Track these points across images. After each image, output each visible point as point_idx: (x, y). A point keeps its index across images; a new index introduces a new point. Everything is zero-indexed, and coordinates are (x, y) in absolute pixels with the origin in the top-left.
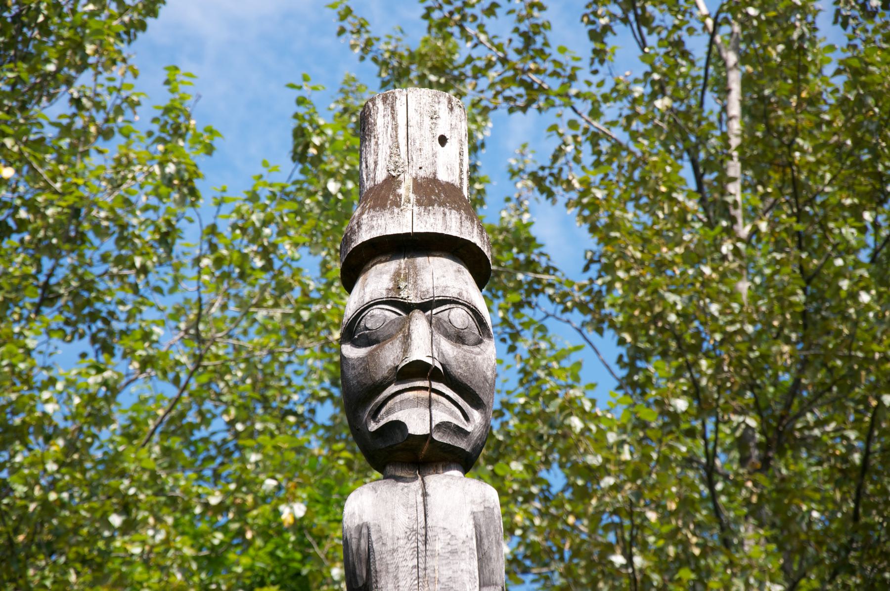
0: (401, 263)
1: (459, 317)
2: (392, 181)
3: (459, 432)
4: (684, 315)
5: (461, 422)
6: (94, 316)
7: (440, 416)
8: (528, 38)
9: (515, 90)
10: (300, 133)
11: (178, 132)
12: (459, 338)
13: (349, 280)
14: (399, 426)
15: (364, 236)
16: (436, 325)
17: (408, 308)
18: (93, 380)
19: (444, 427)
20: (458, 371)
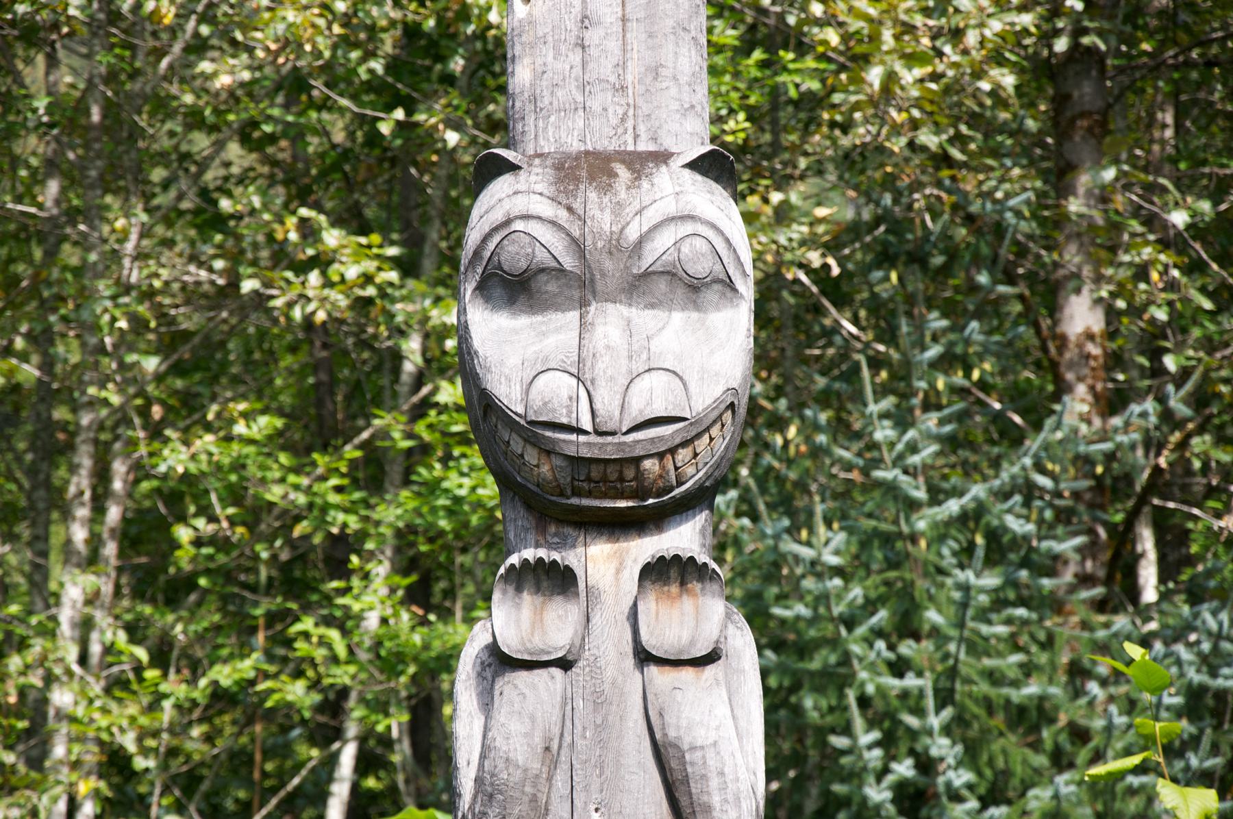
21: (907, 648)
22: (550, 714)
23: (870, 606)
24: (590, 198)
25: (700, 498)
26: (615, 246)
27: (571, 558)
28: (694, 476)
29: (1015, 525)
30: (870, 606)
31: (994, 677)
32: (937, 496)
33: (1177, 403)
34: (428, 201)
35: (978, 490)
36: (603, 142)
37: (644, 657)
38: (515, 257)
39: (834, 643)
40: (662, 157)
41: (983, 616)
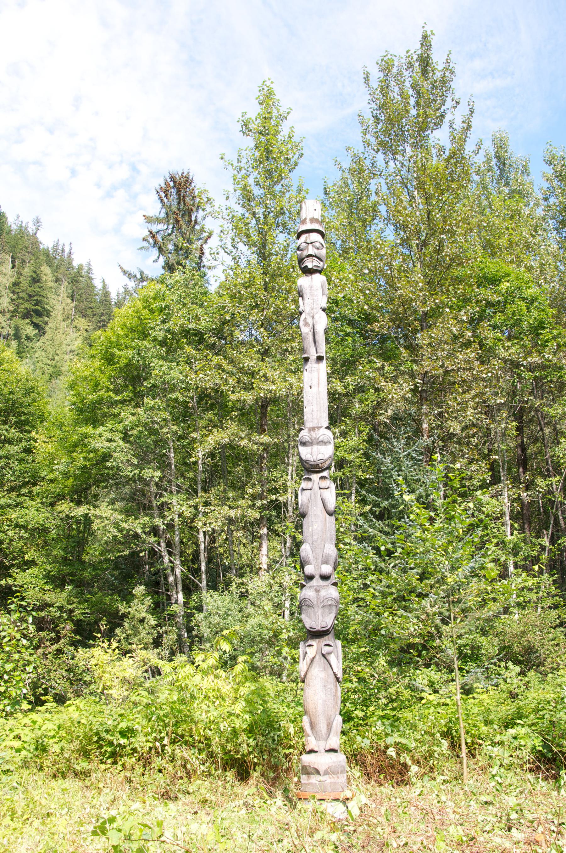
0: (307, 235)
1: (318, 245)
2: (305, 219)
3: (318, 267)
4: (403, 221)
5: (318, 265)
6: (287, 229)
7: (315, 264)
8: (373, 164)
9: (371, 175)
10: (325, 188)
11: (300, 190)
12: (318, 249)
13: (298, 237)
14: (306, 266)
15: (300, 230)
16: (314, 246)
17: (308, 244)
18: (285, 243)
19: (315, 266)
20: (318, 255)
21: (400, 473)
22: (309, 496)
23: (395, 467)
24: (312, 433)
25: (329, 468)
26: (315, 439)
27: (311, 477)
28: (326, 466)
29: (414, 455)
30: (395, 467)
31: (412, 476)
32: (404, 451)
33: (436, 437)
34: (235, 468)
35: (409, 451)
36: (315, 426)
37: (320, 488)
38: (304, 441)
39: (390, 472)
40: (321, 427)
41: (410, 468)
